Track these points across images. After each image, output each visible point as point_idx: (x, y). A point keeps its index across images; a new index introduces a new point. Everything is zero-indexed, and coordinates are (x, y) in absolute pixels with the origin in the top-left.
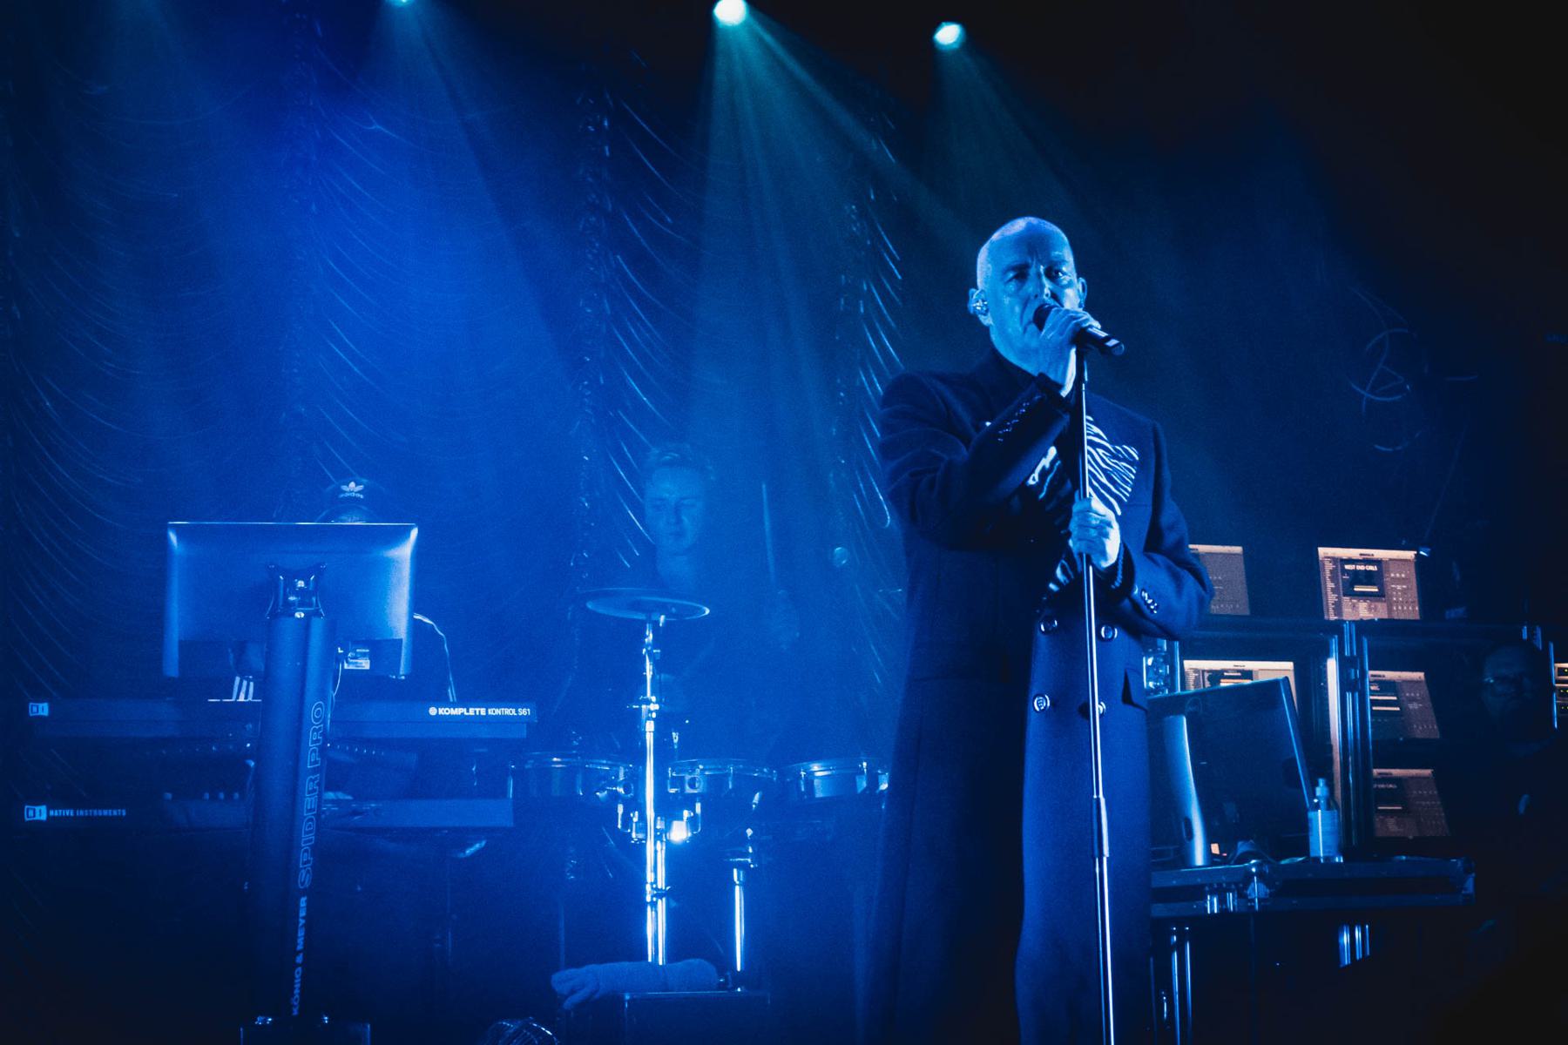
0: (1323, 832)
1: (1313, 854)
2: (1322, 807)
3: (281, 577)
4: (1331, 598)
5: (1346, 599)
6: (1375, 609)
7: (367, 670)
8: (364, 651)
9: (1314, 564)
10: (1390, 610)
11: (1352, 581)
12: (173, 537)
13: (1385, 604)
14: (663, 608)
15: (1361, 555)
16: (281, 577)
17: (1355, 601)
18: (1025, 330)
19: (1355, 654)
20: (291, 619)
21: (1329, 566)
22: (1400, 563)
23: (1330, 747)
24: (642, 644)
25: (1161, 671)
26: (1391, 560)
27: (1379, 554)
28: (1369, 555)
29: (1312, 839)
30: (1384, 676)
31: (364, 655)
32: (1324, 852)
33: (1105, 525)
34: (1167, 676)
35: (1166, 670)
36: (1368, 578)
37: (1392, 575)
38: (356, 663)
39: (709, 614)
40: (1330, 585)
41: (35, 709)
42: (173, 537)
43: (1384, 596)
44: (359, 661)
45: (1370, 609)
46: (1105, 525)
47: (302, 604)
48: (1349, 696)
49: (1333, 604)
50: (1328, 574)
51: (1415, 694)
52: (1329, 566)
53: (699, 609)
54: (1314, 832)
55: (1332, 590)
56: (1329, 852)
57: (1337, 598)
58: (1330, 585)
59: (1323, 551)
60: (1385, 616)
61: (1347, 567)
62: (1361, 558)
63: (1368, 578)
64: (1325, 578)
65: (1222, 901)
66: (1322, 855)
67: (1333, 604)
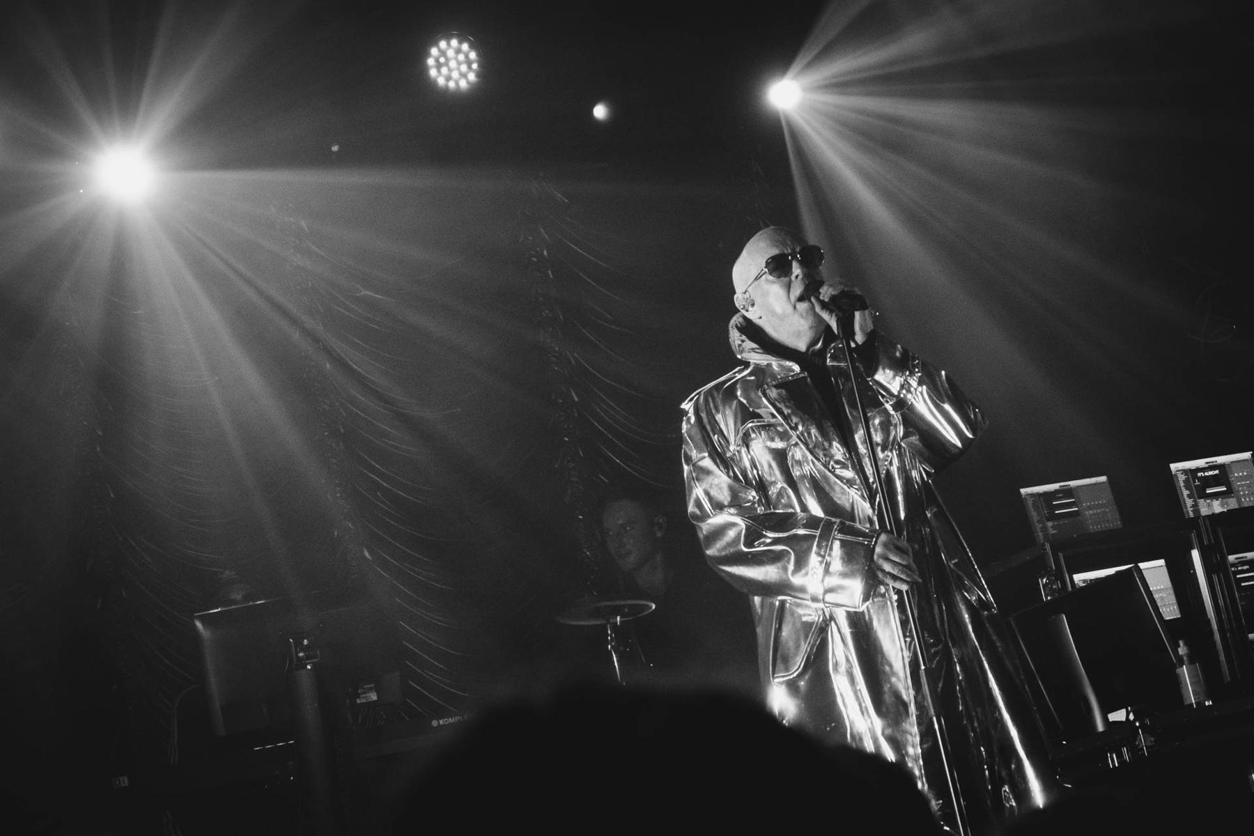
0: (1190, 683)
1: (1187, 703)
2: (1186, 663)
3: (291, 640)
4: (1189, 502)
5: (1201, 501)
6: (1227, 504)
7: (375, 701)
8: (369, 686)
9: (1170, 478)
10: (1239, 501)
11: (1200, 485)
12: (199, 624)
13: (1235, 499)
14: (617, 610)
15: (1207, 463)
16: (291, 640)
17: (1208, 501)
18: (795, 307)
19: (1213, 541)
20: (304, 671)
21: (1182, 478)
22: (1238, 464)
23: (1208, 621)
24: (607, 643)
25: (1054, 587)
26: (1231, 462)
27: (1220, 460)
28: (1213, 462)
29: (1183, 691)
30: (1246, 557)
31: (371, 689)
32: (1195, 699)
33: (741, 396)
34: (1059, 590)
35: (1058, 584)
36: (1215, 481)
37: (1236, 475)
38: (366, 697)
39: (655, 609)
40: (1186, 493)
41: (117, 783)
42: (199, 624)
43: (1233, 493)
44: (367, 695)
45: (1222, 505)
46: (741, 396)
47: (308, 657)
48: (1215, 578)
49: (1191, 507)
50: (1182, 484)
51: (1102, 501)
52: (1182, 478)
53: (647, 606)
54: (1183, 685)
55: (1188, 495)
56: (1199, 698)
57: (1193, 501)
58: (1186, 493)
59: (1174, 467)
60: (1237, 507)
61: (1199, 474)
62: (1207, 466)
63: (1215, 481)
64: (1180, 487)
65: (1120, 756)
66: (1193, 701)
67: (1191, 507)
